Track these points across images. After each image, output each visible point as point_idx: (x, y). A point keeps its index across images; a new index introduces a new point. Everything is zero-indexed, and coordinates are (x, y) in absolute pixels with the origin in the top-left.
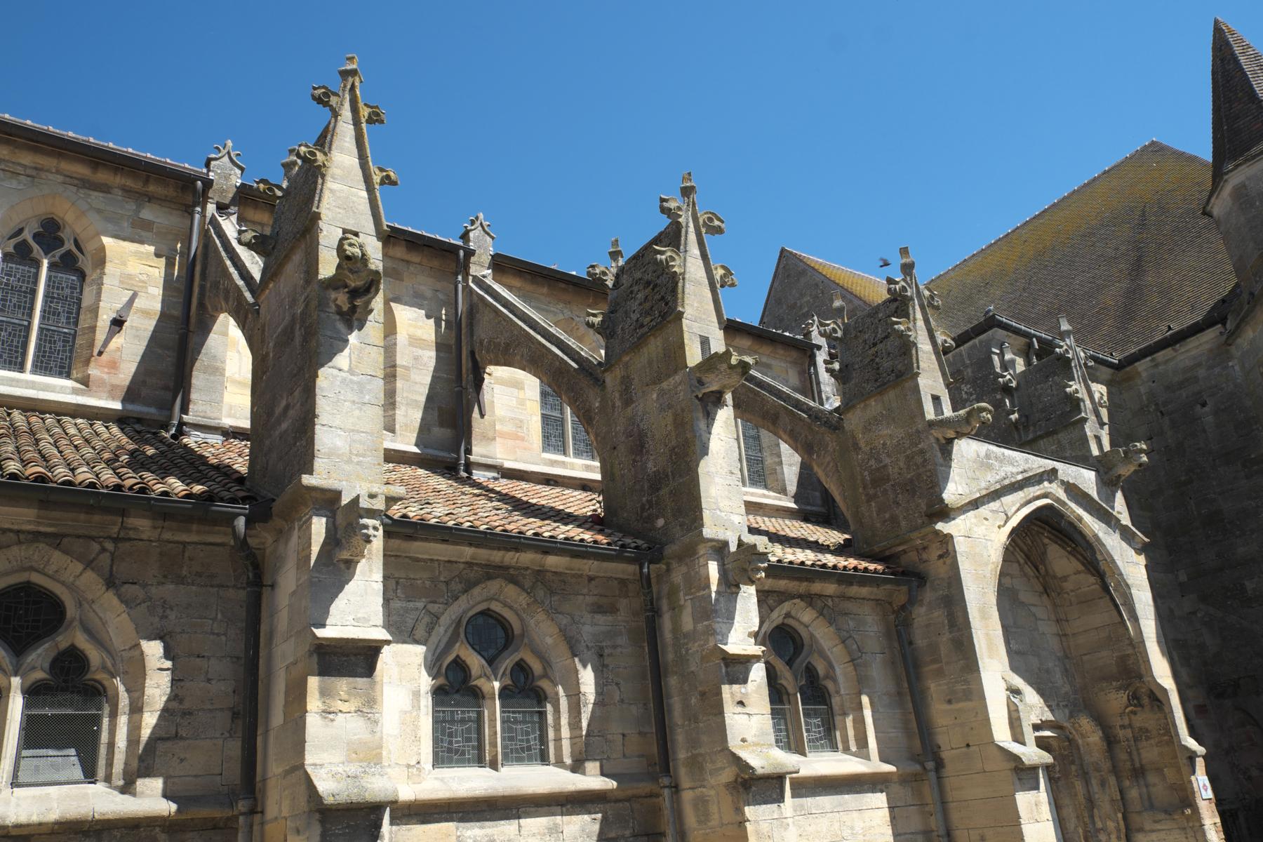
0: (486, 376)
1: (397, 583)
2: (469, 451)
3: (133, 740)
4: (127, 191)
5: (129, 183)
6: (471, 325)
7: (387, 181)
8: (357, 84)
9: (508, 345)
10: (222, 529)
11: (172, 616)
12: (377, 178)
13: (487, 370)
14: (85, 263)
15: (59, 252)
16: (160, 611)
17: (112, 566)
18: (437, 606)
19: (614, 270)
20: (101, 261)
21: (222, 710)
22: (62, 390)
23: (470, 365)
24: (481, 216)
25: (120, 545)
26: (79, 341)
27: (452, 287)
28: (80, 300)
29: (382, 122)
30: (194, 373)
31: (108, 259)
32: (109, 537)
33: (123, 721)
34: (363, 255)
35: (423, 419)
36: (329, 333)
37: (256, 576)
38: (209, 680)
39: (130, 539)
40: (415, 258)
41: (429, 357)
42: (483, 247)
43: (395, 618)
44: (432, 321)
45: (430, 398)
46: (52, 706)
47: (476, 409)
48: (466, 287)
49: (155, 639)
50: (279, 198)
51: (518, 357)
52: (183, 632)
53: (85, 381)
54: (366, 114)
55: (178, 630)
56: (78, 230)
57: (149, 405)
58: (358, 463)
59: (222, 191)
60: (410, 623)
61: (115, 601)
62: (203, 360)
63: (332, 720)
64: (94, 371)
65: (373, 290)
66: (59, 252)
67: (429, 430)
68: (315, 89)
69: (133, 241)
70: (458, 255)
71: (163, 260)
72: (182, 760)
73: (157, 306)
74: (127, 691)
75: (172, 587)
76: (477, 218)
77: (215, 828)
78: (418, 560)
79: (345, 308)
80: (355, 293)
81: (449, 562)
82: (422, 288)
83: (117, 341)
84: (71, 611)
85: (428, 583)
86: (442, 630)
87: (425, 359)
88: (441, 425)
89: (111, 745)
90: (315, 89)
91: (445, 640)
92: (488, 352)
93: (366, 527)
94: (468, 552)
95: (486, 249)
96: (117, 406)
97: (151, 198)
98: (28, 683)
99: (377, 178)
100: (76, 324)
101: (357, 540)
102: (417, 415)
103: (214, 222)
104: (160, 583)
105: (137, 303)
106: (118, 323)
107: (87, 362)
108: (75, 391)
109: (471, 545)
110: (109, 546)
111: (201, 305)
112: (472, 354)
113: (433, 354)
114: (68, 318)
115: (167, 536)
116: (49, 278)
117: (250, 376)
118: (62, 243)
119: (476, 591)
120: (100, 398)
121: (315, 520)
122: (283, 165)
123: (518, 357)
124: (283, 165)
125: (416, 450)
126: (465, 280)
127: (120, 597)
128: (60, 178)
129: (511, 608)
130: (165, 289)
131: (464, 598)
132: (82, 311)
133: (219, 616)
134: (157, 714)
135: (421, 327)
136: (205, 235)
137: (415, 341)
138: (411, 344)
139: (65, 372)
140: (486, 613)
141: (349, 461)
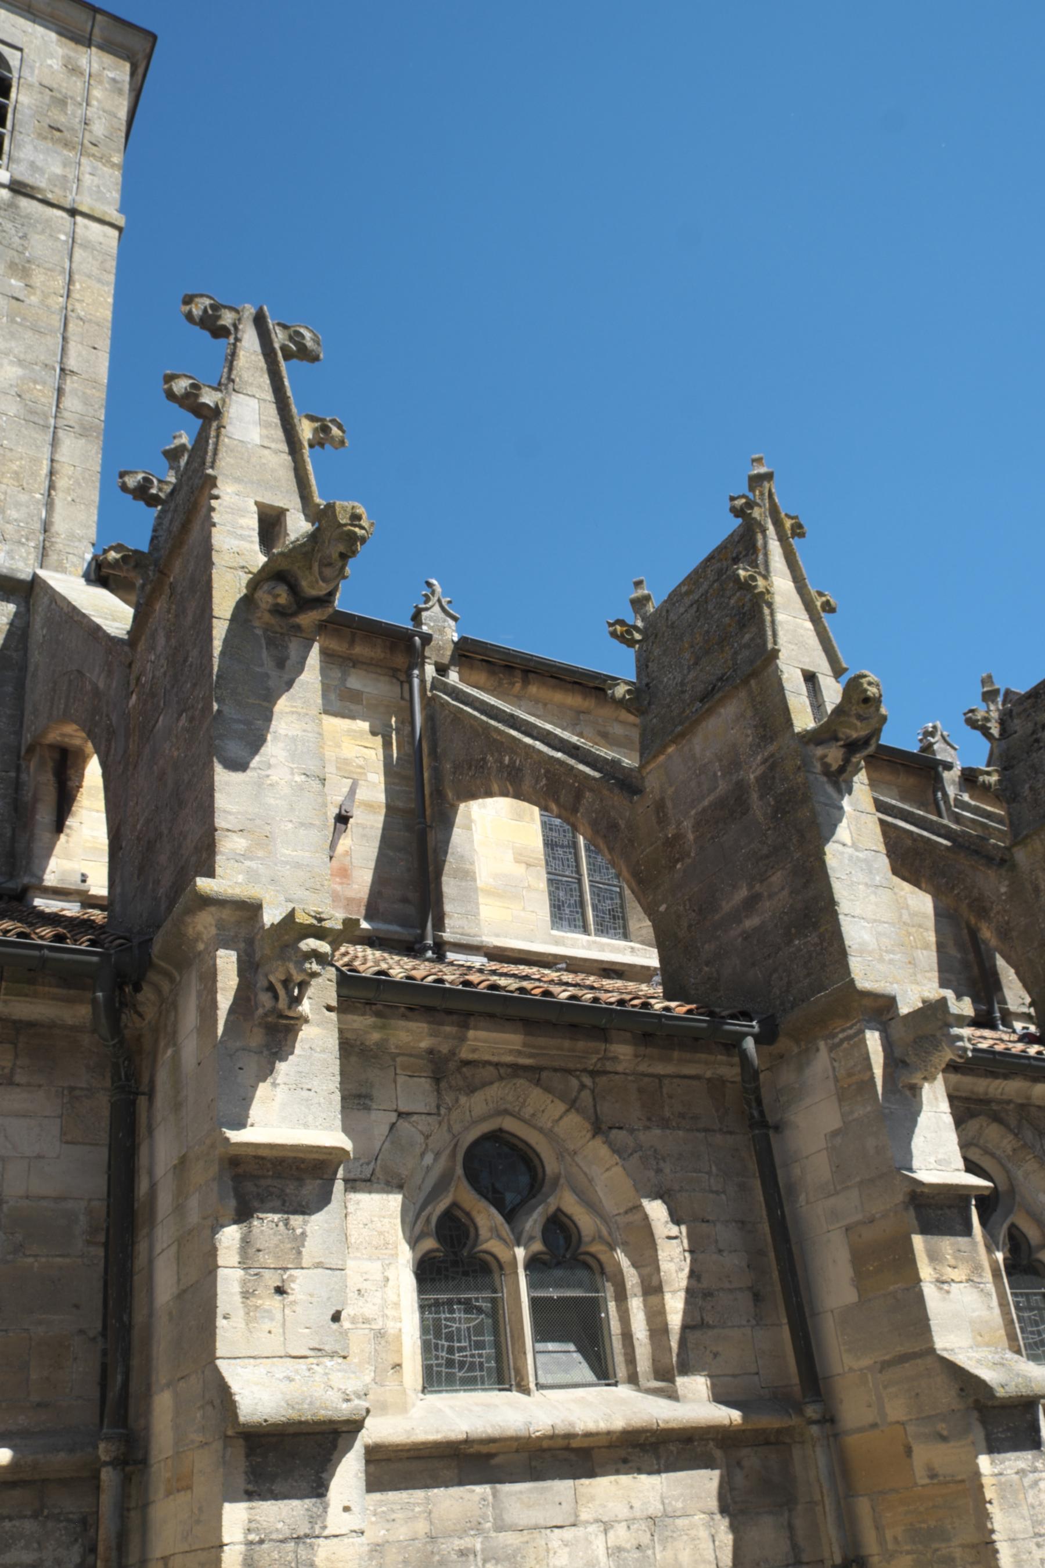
3: (658, 1329)
10: (703, 1056)
11: (667, 1168)
17: (595, 1106)
19: (995, 715)
21: (740, 1289)
25: (597, 1080)
32: (585, 1070)
33: (636, 1305)
38: (720, 1251)
46: (557, 1285)
50: (638, 642)
52: (681, 1190)
55: (676, 1187)
57: (390, 922)
59: (440, 648)
61: (604, 1151)
62: (451, 862)
63: (948, 1292)
68: (732, 499)
69: (343, 716)
72: (716, 1355)
73: (381, 797)
74: (634, 1265)
75: (658, 1132)
77: (767, 1443)
84: (551, 1165)
89: (627, 1336)
93: (960, 1038)
98: (530, 1253)
110: (587, 1080)
129: (993, 1155)
134: (682, 1295)
136: (429, 703)
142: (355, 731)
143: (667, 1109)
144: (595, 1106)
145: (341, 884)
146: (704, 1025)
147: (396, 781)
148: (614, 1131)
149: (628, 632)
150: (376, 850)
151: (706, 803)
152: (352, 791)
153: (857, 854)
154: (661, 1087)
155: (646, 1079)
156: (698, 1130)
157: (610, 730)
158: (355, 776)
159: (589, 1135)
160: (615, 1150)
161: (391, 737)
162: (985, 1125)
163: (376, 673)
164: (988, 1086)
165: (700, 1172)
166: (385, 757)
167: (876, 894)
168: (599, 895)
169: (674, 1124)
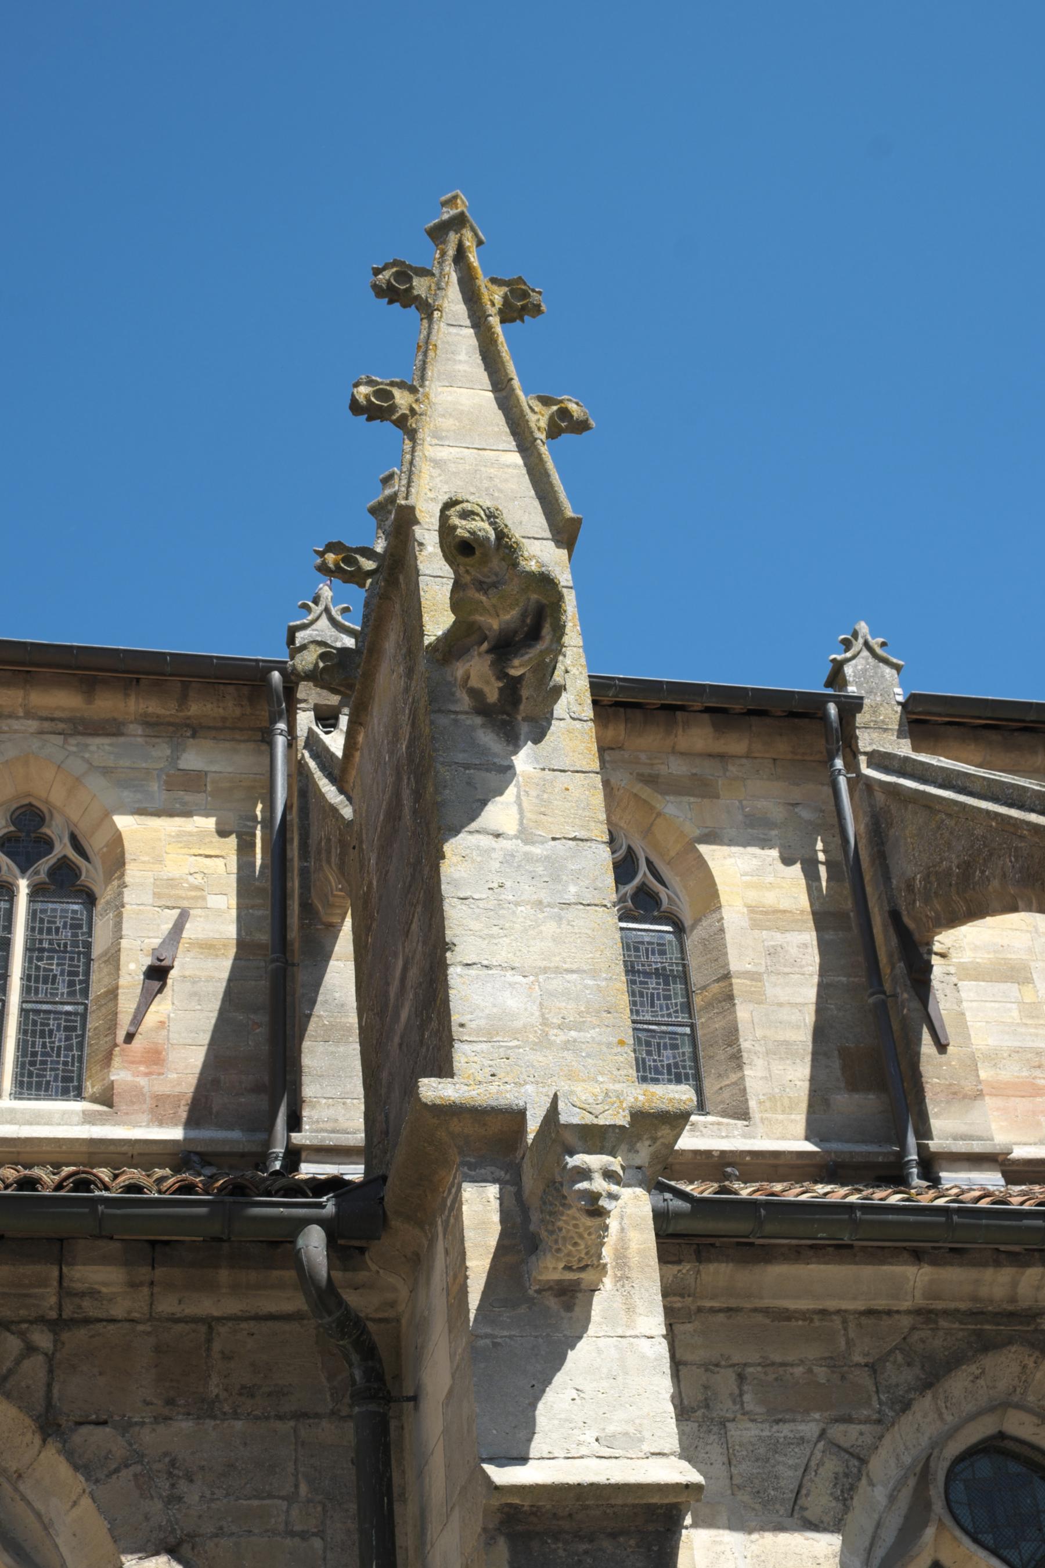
0: (935, 960)
1: (741, 1378)
2: (924, 1132)
4: (153, 725)
5: (153, 707)
6: (881, 857)
7: (563, 424)
8: (469, 242)
9: (967, 867)
11: (192, 1494)
12: (538, 419)
13: (937, 947)
14: (91, 874)
15: (45, 864)
16: (164, 1484)
17: (49, 1386)
18: (854, 1429)
20: (116, 860)
22: (64, 1119)
23: (894, 941)
24: (863, 628)
25: (65, 1336)
26: (93, 1023)
27: (827, 790)
28: (88, 945)
29: (536, 310)
30: (306, 1044)
31: (128, 857)
32: (41, 1320)
34: (501, 535)
35: (813, 1079)
36: (460, 757)
37: (377, 1380)
39: (87, 1321)
40: (735, 744)
41: (803, 946)
42: (880, 692)
43: (745, 1468)
44: (797, 869)
45: (820, 1033)
47: (926, 1036)
48: (858, 782)
49: (157, 1553)
50: (370, 574)
51: (996, 883)
52: (219, 1533)
53: (106, 1098)
54: (498, 299)
56: (74, 817)
57: (230, 1127)
58: (566, 1046)
60: (789, 1478)
61: (64, 1470)
64: (120, 1075)
65: (546, 630)
66: (45, 864)
67: (826, 1102)
68: (377, 272)
69: (171, 814)
70: (825, 717)
71: (232, 841)
73: (230, 930)
75: (187, 1425)
76: (855, 635)
78: (786, 1315)
79: (492, 695)
80: (504, 648)
81: (870, 1312)
82: (761, 804)
83: (161, 1008)
85: (821, 1373)
86: (880, 1494)
87: (793, 951)
88: (853, 1085)
90: (377, 272)
91: (894, 1523)
92: (927, 901)
93: (585, 1174)
94: (914, 1280)
95: (886, 693)
96: (176, 1133)
97: (195, 729)
99: (538, 419)
100: (85, 992)
101: (573, 1219)
102: (798, 1075)
103: (313, 743)
104: (158, 1419)
105: (189, 931)
106: (158, 973)
107: (108, 1059)
108: (89, 1118)
109: (918, 1256)
110: (42, 1339)
111: (307, 907)
112: (895, 916)
113: (810, 937)
114: (71, 984)
115: (167, 1305)
116: (33, 915)
117: (351, 948)
118: (48, 845)
119: (958, 1384)
120: (136, 1125)
121: (470, 1192)
122: (373, 511)
123: (996, 883)
124: (373, 511)
125: (809, 1147)
126: (852, 765)
127: (70, 1455)
128: (33, 725)
130: (240, 894)
131: (924, 1404)
132: (94, 966)
133: (303, 1489)
135: (771, 886)
137: (764, 918)
138: (756, 925)
139: (70, 1087)
140: (996, 1446)
141: (543, 1043)
142: (190, 834)
143: (215, 1380)
144: (49, 1386)
145: (147, 1074)
146: (203, 1210)
147: (259, 901)
148: (84, 1430)
149: (349, 560)
150: (215, 1014)
151: (382, 817)
152: (178, 927)
153: (528, 848)
154: (209, 1340)
155: (180, 1327)
156: (280, 1417)
157: (663, 770)
158: (185, 904)
159: (37, 1440)
160: (82, 1467)
161: (254, 835)
162: (1030, 1363)
163: (233, 740)
164: (1015, 1284)
165: (270, 1496)
166: (240, 868)
167: (560, 919)
168: (648, 1044)
169: (227, 1408)
